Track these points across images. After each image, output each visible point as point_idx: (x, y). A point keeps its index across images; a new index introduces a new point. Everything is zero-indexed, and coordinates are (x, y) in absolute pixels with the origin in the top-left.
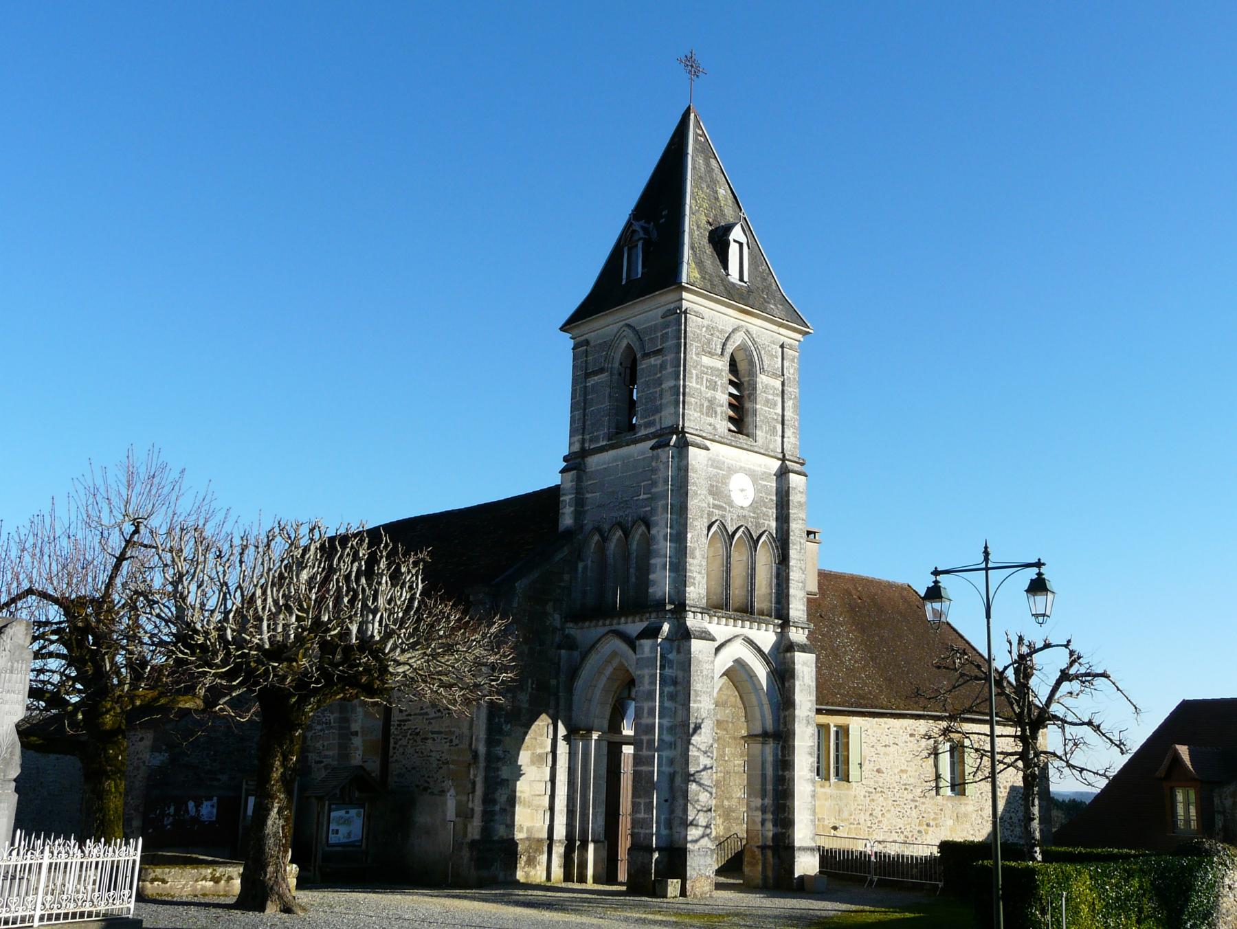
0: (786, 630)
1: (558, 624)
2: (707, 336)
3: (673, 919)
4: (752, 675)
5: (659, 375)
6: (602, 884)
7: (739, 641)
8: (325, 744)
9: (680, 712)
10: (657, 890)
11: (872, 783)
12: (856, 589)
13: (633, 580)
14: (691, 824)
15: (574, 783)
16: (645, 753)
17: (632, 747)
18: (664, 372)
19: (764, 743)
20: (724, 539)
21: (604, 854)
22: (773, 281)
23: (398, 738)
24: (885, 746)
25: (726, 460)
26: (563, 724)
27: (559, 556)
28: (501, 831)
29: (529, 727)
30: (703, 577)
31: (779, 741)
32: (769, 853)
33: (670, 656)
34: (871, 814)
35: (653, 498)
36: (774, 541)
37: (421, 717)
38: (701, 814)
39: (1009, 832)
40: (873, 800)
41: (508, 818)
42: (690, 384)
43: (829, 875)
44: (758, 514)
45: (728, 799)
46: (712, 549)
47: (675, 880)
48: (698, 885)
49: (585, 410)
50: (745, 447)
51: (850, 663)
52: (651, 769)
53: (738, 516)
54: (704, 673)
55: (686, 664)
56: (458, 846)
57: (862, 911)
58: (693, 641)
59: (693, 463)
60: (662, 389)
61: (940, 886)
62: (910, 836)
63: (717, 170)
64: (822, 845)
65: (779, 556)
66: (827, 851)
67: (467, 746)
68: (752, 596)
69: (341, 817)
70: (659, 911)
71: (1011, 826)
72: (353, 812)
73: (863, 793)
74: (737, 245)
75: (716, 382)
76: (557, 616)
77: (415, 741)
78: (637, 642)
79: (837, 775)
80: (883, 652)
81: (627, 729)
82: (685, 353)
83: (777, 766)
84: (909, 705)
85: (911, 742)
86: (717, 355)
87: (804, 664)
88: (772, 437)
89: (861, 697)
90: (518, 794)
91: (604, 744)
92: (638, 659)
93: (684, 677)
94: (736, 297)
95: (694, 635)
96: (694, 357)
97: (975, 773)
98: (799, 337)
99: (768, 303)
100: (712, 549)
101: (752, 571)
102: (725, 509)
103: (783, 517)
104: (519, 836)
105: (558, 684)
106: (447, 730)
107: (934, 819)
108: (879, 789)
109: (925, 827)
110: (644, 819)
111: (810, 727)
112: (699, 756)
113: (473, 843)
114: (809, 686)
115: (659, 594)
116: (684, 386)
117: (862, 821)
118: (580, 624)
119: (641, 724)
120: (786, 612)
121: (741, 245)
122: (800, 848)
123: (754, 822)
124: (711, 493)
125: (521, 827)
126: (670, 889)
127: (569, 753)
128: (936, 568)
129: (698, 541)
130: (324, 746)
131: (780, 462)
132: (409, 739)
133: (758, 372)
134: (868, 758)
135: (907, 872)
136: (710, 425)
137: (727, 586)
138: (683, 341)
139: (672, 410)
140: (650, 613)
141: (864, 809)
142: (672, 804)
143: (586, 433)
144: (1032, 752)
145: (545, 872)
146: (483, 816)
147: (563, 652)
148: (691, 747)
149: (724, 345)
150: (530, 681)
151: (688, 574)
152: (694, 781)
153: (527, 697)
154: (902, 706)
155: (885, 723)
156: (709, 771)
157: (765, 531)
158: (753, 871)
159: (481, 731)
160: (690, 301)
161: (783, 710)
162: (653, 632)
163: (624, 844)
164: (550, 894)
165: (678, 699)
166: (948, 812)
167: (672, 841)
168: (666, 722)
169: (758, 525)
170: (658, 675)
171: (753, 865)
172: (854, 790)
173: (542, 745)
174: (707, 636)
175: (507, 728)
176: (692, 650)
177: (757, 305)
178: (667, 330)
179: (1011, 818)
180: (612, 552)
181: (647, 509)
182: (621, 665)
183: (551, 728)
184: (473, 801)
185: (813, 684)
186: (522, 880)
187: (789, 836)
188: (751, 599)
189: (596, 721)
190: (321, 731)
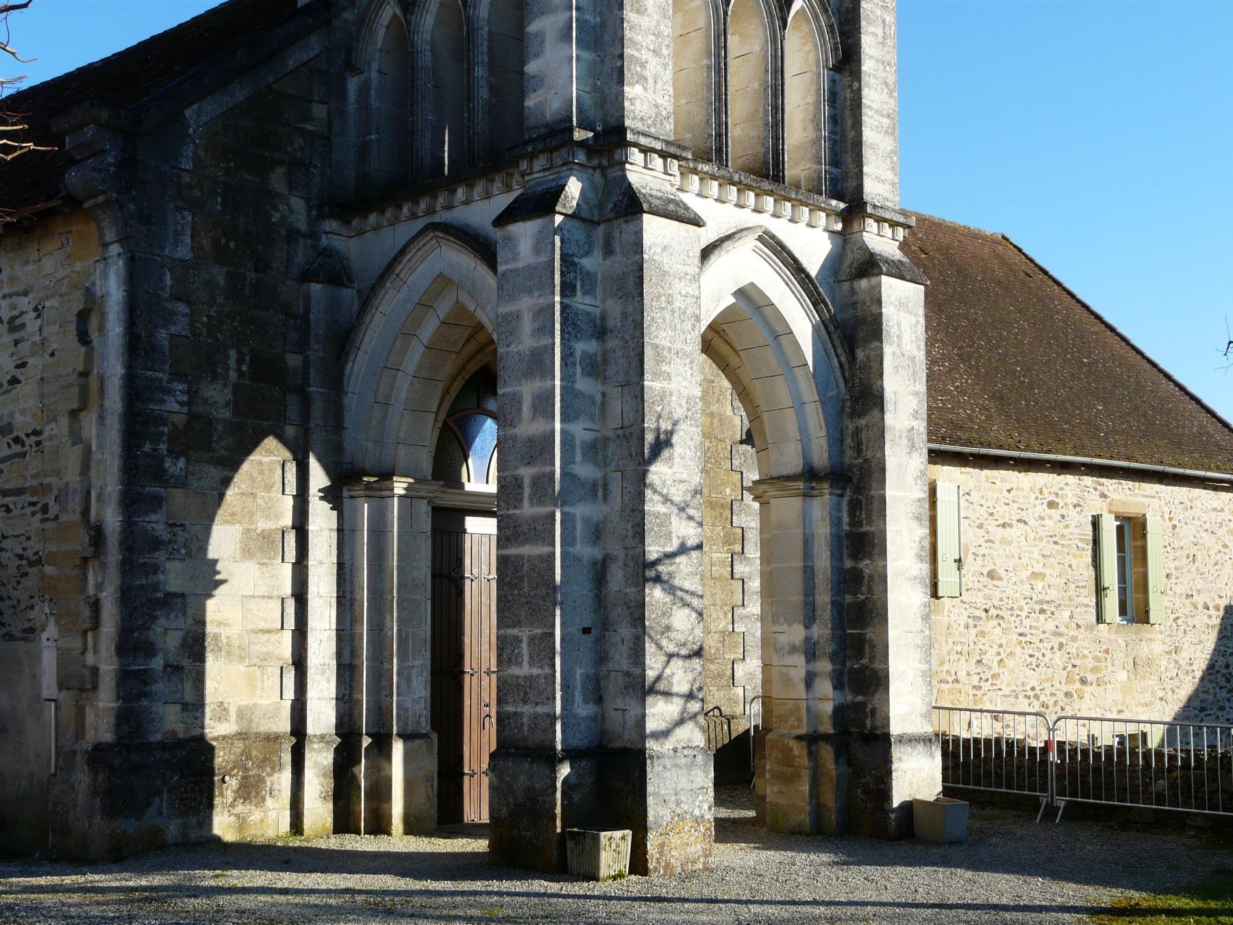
0: (856, 227)
1: (301, 223)
4: (779, 332)
6: (429, 834)
9: (616, 407)
11: (980, 600)
13: (483, 93)
14: (652, 691)
15: (353, 600)
16: (527, 510)
19: (807, 495)
21: (430, 764)
24: (1004, 525)
26: (320, 460)
27: (296, 57)
28: (170, 720)
30: (665, 66)
31: (844, 488)
32: (827, 752)
33: (587, 263)
34: (979, 662)
38: (677, 664)
40: (983, 634)
41: (188, 686)
47: (618, 834)
48: (675, 840)
52: (546, 550)
54: (677, 305)
56: (66, 757)
58: (647, 218)
62: (1051, 704)
64: (942, 729)
65: (835, 49)
67: (77, 517)
73: (963, 619)
76: (297, 203)
80: (981, 347)
81: (476, 481)
83: (840, 548)
85: (1050, 517)
87: (902, 305)
90: (210, 629)
91: (424, 509)
100: (680, 14)
104: (215, 728)
106: (35, 483)
107: (1095, 670)
108: (993, 612)
109: (1078, 685)
110: (530, 678)
111: (916, 455)
112: (667, 516)
113: (98, 754)
117: (962, 676)
119: (514, 438)
122: (902, 739)
123: (787, 681)
125: (222, 707)
127: (340, 530)
134: (972, 550)
140: (532, 157)
142: (600, 640)
145: (288, 812)
146: (118, 685)
147: (315, 288)
148: (648, 493)
150: (233, 354)
152: (658, 579)
153: (228, 394)
155: (1003, 480)
156: (694, 554)
161: (851, 416)
162: (544, 201)
164: (287, 879)
165: (612, 370)
166: (1119, 655)
167: (603, 732)
168: (580, 431)
170: (558, 307)
171: (788, 779)
172: (946, 613)
173: (270, 511)
175: (175, 467)
180: (427, 37)
183: (292, 469)
184: (96, 650)
186: (229, 836)
187: (873, 711)
189: (402, 451)
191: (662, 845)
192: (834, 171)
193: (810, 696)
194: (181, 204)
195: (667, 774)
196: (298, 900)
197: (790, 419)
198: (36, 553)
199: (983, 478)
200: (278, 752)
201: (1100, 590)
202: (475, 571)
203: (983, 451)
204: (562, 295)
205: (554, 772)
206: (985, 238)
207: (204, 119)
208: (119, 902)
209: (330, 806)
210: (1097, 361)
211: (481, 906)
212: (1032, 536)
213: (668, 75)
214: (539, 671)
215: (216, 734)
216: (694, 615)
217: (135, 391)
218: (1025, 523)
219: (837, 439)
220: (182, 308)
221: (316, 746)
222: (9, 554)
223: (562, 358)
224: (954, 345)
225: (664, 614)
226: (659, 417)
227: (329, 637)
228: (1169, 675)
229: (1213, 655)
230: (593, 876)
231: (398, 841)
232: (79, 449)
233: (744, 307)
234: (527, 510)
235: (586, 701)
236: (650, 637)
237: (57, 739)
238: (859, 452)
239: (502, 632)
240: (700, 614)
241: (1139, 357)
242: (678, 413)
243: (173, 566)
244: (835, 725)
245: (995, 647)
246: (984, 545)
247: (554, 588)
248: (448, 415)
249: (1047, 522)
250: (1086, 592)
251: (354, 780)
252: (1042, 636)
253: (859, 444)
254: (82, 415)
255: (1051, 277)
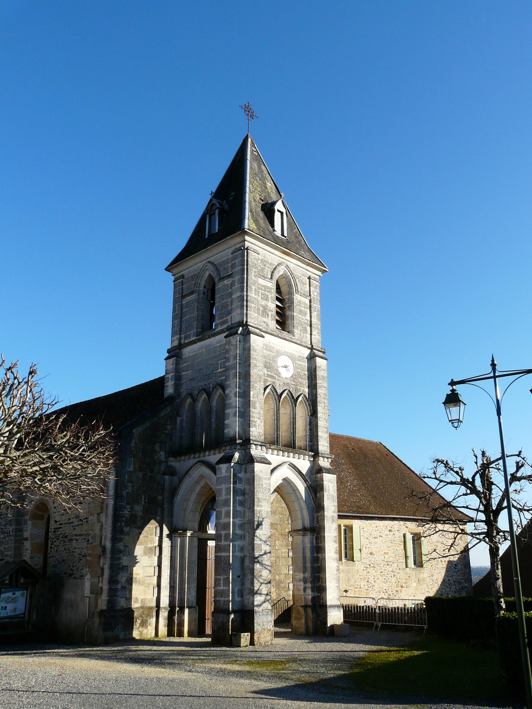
0: (317, 459)
1: (163, 458)
2: (262, 266)
3: (247, 668)
4: (295, 489)
5: (230, 290)
6: (195, 637)
7: (285, 468)
8: (6, 547)
9: (247, 514)
10: (234, 642)
11: (367, 562)
12: (351, 444)
13: (214, 426)
14: (256, 593)
15: (174, 567)
16: (223, 543)
17: (214, 541)
18: (233, 288)
20: (275, 398)
21: (196, 616)
22: (302, 239)
23: (54, 540)
24: (375, 538)
25: (275, 347)
26: (166, 526)
28: (122, 603)
29: (142, 528)
30: (262, 422)
31: (314, 533)
32: (310, 611)
33: (240, 475)
35: (227, 369)
36: (308, 401)
37: (69, 525)
38: (263, 585)
39: (448, 589)
40: (369, 572)
41: (127, 593)
42: (251, 295)
43: (350, 623)
44: (296, 382)
45: (278, 575)
46: (267, 405)
47: (246, 634)
48: (262, 636)
49: (181, 318)
50: (288, 338)
51: (351, 487)
52: (228, 554)
53: (284, 383)
54: (264, 486)
55: (251, 480)
56: (92, 614)
57: (381, 651)
59: (254, 345)
60: (232, 299)
61: (425, 628)
62: (391, 594)
63: (266, 172)
65: (311, 411)
66: (346, 606)
67: (98, 543)
68: (294, 437)
69: (9, 597)
70: (236, 661)
71: (450, 585)
72: (18, 593)
73: (362, 568)
74: (279, 214)
75: (267, 296)
76: (162, 453)
77: (65, 542)
78: (217, 467)
79: (346, 557)
81: (211, 530)
82: (247, 275)
84: (388, 512)
85: (390, 535)
86: (268, 278)
87: (329, 481)
88: (304, 334)
89: (359, 507)
90: (134, 576)
91: (196, 540)
92: (218, 478)
93: (250, 490)
94: (280, 243)
95: (256, 460)
96: (253, 277)
97: (449, 549)
98: (319, 273)
99: (300, 250)
100: (267, 405)
101: (293, 420)
102: (275, 378)
103: (313, 385)
104: (135, 605)
105: (163, 498)
106: (85, 533)
108: (372, 565)
109: (400, 588)
110: (223, 590)
111: (334, 523)
112: (261, 544)
114: (333, 496)
115: (232, 433)
116: (247, 296)
117: (362, 586)
118: (178, 458)
119: (220, 523)
120: (316, 447)
121: (282, 213)
122: (330, 606)
123: (298, 589)
124: (266, 367)
125: (137, 599)
126: (243, 641)
127: (171, 546)
128: (452, 380)
129: (257, 397)
130: (5, 549)
131: (310, 351)
132: (61, 541)
133: (295, 292)
134: (365, 546)
135: (402, 618)
136: (264, 323)
137: (278, 429)
138: (246, 267)
139: (239, 311)
140: (226, 446)
141: (363, 579)
142: (243, 579)
143: (182, 333)
144: (495, 531)
145: (154, 630)
146: (108, 593)
148: (255, 538)
149: (272, 272)
151: (251, 419)
152: (258, 562)
153: (141, 508)
154: (384, 513)
155: (374, 523)
156: (269, 555)
157: (301, 394)
158: (298, 623)
159: (108, 533)
160: (250, 242)
162: (228, 459)
163: (210, 608)
164: (155, 648)
166: (413, 578)
167: (243, 605)
168: (237, 521)
169: (297, 390)
170: (232, 488)
171: (299, 619)
173: (152, 541)
174: (266, 462)
175: (126, 529)
176: (256, 470)
177: (292, 250)
178: (235, 261)
179: (449, 580)
180: (200, 409)
181: (222, 378)
182: (206, 484)
183: (158, 529)
185: (335, 495)
186: (137, 638)
187: (322, 598)
188: (294, 438)
189: (190, 524)
190: (4, 538)
191: (259, 637)
192: (311, 443)
193: (305, 594)
194: (131, 456)
195: (260, 617)
196: (159, 652)
197: (299, 513)
198: (85, 553)
199: (368, 523)
200: (152, 612)
201: (406, 557)
202: (210, 557)
203: (367, 515)
204: (233, 484)
205: (229, 617)
206: (374, 443)
207: (138, 432)
208: (111, 653)
209: (167, 628)
210: (407, 483)
211: (208, 653)
212: (384, 541)
213: (262, 424)
214: (226, 588)
215: (134, 607)
216: (268, 572)
217: (116, 508)
218: (382, 537)
219: (312, 519)
220: (130, 484)
221: (163, 610)
222: (77, 553)
223: (233, 502)
224: (361, 480)
225: (260, 572)
226: (259, 517)
227: (167, 578)
228: (430, 584)
229: (444, 577)
230: (239, 646)
231: (186, 639)
232: (99, 524)
233: (285, 483)
234: (223, 543)
235: (238, 596)
236: (256, 578)
237: (89, 608)
238: (318, 523)
239: (216, 577)
240: (270, 571)
241: (422, 481)
242: (264, 516)
243: (125, 558)
244: (312, 602)
245: (373, 576)
246: (368, 544)
247: (230, 564)
248: (203, 511)
249: (389, 536)
250: (402, 558)
251: (174, 620)
252: (388, 573)
253: (318, 520)
254: (101, 514)
255: (395, 456)
